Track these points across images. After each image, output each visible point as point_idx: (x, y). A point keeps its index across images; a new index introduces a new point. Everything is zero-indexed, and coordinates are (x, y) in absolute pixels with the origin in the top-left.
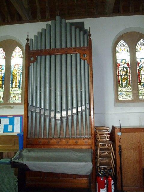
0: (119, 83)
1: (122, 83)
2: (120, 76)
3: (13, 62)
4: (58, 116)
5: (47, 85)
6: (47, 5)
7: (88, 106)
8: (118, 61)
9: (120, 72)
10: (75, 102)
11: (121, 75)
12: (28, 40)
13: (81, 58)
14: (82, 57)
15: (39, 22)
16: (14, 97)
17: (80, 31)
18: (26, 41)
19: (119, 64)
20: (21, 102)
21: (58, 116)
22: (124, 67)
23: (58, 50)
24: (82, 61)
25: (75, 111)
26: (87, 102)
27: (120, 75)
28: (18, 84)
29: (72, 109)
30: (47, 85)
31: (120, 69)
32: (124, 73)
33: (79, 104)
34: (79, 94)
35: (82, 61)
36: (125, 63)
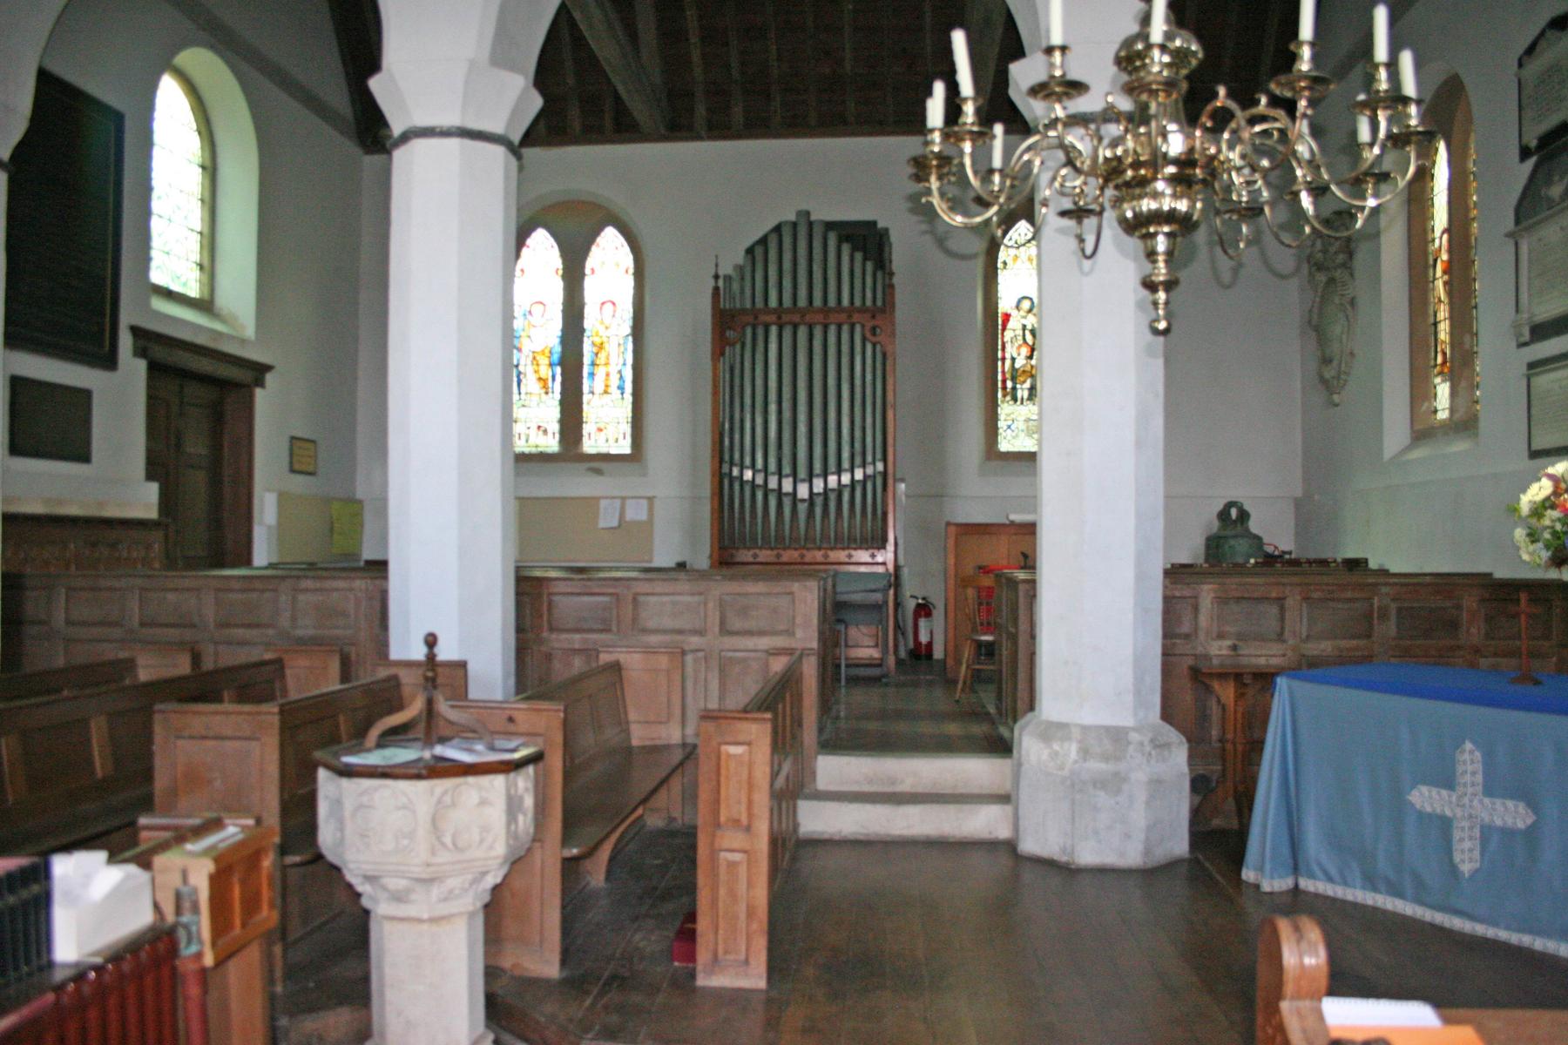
0: (1004, 388)
1: (1014, 389)
2: (1008, 363)
3: (593, 290)
4: (803, 491)
5: (773, 408)
6: (735, 74)
7: (880, 466)
8: (1005, 304)
9: (1008, 346)
10: (846, 455)
11: (1013, 359)
12: (716, 277)
13: (864, 339)
14: (868, 335)
15: (699, 138)
16: (600, 430)
17: (865, 259)
18: (712, 283)
19: (1007, 317)
20: (627, 450)
21: (803, 491)
22: (1024, 327)
23: (802, 313)
24: (869, 347)
25: (846, 479)
26: (879, 456)
27: (1008, 356)
28: (614, 381)
29: (825, 475)
30: (773, 408)
31: (1008, 335)
32: (1025, 351)
33: (858, 460)
34: (858, 434)
35: (869, 347)
36: (1030, 311)
